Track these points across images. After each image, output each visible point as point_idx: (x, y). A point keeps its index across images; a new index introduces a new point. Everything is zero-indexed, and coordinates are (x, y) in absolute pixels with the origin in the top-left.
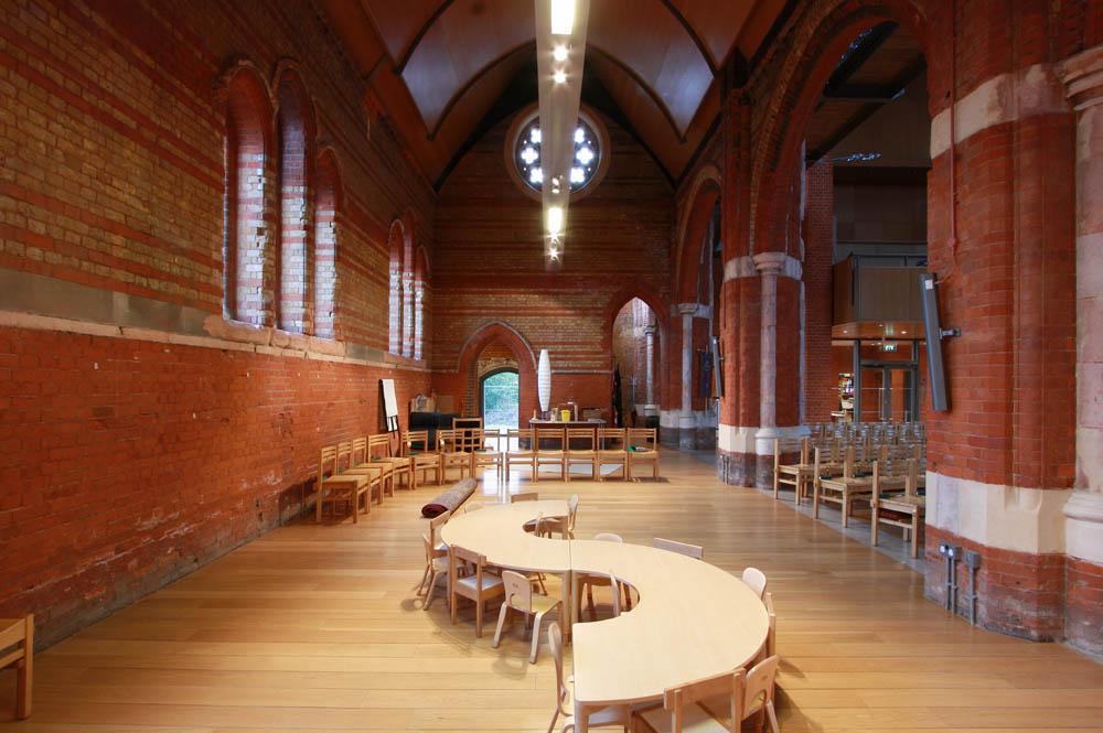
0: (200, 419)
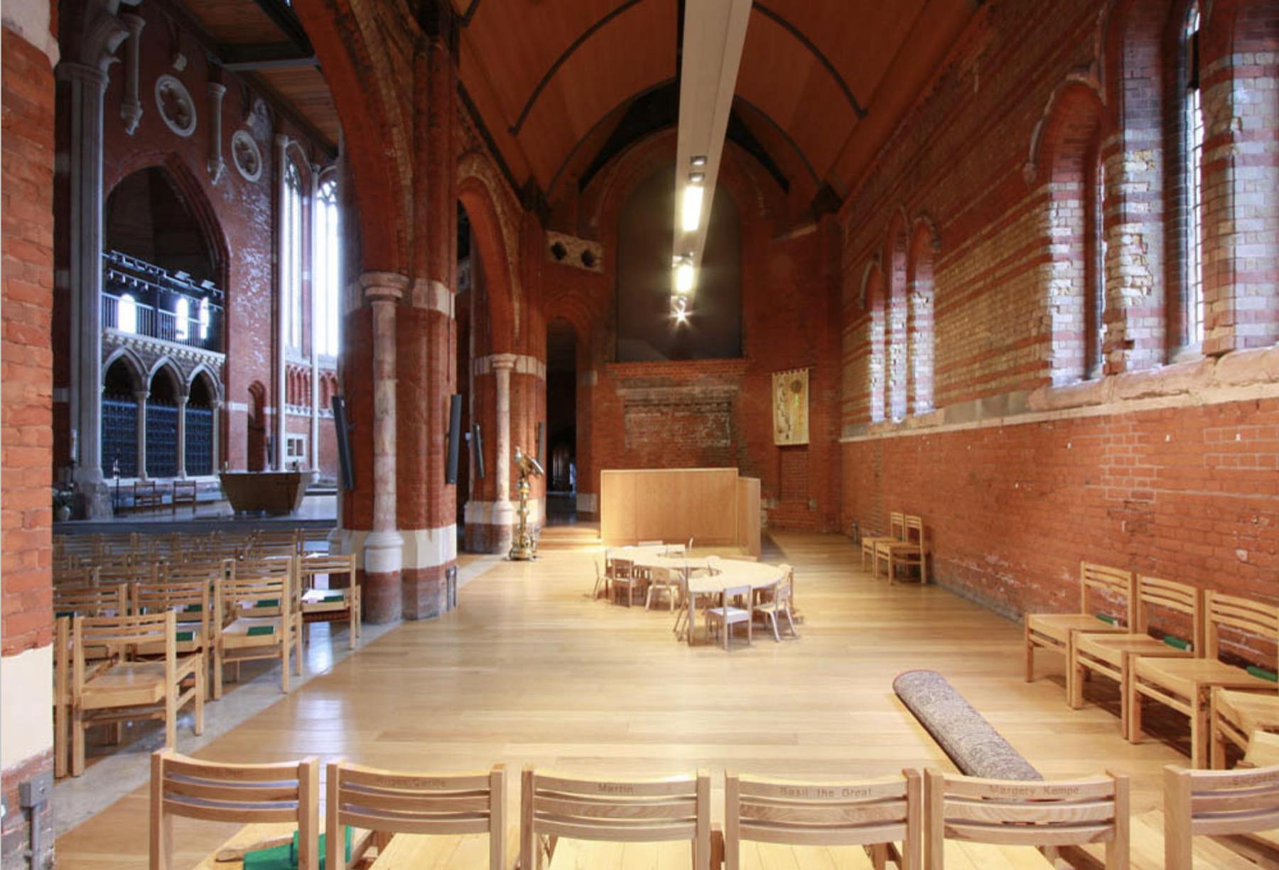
0: (1021, 489)
